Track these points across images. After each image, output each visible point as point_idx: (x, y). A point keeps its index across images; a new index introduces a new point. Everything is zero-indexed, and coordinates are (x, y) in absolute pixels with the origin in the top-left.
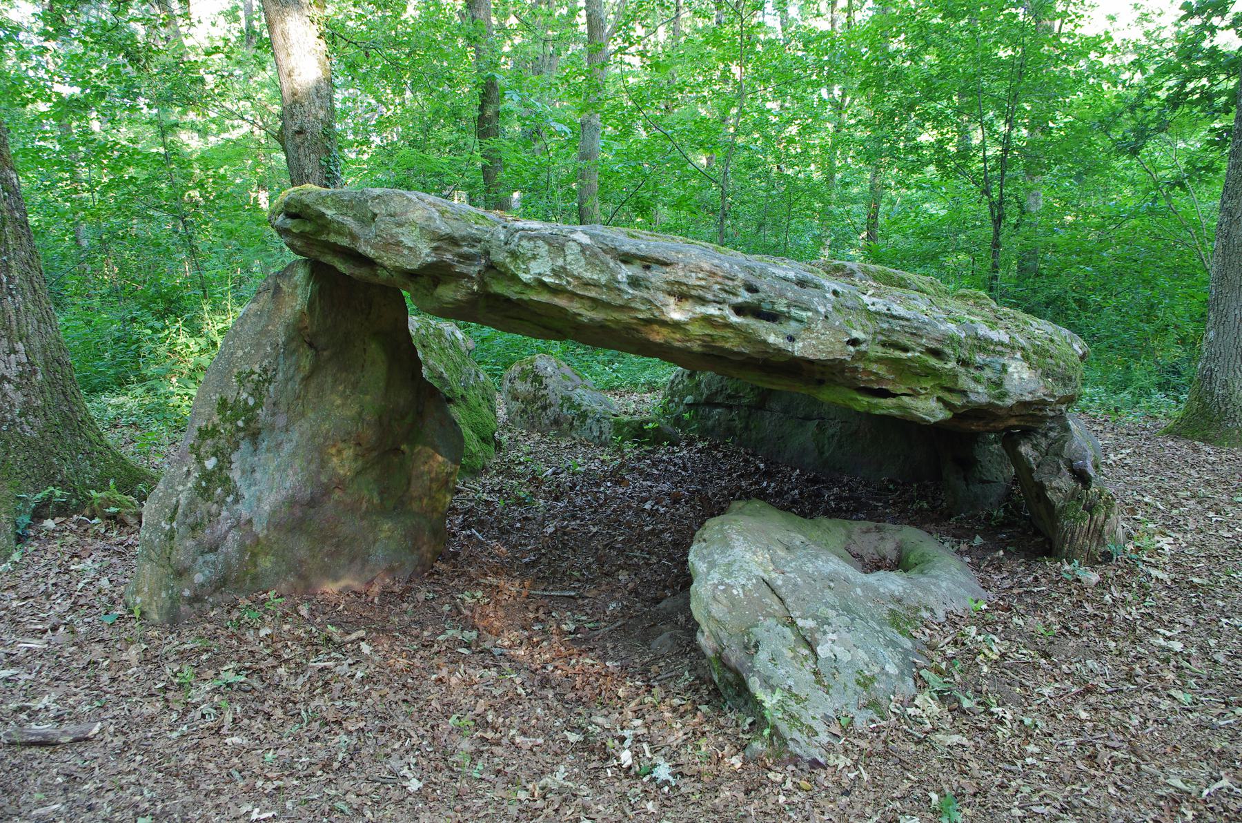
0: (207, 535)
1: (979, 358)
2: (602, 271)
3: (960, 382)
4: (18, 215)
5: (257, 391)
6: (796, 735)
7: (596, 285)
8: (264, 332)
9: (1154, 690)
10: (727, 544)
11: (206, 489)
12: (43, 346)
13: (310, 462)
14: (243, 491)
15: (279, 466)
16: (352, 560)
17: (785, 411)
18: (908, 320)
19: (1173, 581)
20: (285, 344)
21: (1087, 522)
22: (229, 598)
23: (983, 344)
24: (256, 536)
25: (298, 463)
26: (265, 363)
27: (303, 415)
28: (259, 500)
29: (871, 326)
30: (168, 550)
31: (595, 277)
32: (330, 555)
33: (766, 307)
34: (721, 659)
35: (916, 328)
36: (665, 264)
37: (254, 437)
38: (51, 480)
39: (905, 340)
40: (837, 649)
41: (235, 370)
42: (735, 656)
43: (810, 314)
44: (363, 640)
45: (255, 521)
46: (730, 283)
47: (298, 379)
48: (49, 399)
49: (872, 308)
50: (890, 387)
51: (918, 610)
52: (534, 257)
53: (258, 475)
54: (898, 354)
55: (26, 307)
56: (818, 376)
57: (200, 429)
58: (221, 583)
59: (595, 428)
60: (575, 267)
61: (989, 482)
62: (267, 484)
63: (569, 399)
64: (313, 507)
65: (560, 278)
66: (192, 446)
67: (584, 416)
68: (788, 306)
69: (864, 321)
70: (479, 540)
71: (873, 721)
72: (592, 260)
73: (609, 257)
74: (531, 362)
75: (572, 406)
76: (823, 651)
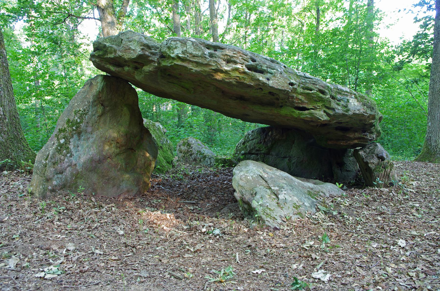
0: (59, 167)
1: (339, 96)
2: (199, 51)
3: (332, 105)
4: (5, 65)
5: (81, 117)
6: (269, 219)
7: (197, 56)
8: (85, 98)
9: (407, 214)
10: (247, 165)
11: (60, 150)
12: (9, 110)
13: (99, 146)
14: (74, 153)
15: (88, 146)
16: (114, 186)
17: (277, 155)
18: (312, 79)
19: (416, 192)
20: (93, 102)
21: (384, 172)
22: (66, 193)
23: (340, 92)
24: (78, 170)
25: (95, 146)
26: (85, 107)
27: (98, 129)
28: (79, 157)
29: (298, 80)
30: (44, 171)
31: (197, 53)
32: (106, 183)
33: (259, 67)
34: (242, 199)
35: (315, 82)
36: (222, 49)
37: (79, 134)
38: (8, 157)
39: (311, 86)
40: (286, 196)
41: (74, 110)
42: (247, 197)
43: (275, 71)
44: (113, 207)
45: (77, 165)
46: (245, 57)
47: (97, 115)
48: (10, 129)
49: (299, 74)
50: (306, 106)
51: (319, 192)
52: (176, 48)
53: (80, 148)
54: (308, 91)
55: (5, 96)
56: (281, 105)
57: (59, 129)
58: (63, 186)
59: (209, 161)
60: (190, 50)
61: (349, 171)
62: (83, 152)
63: (200, 151)
64: (100, 163)
65: (185, 54)
66: (56, 135)
67: (205, 157)
68: (267, 67)
69: (295, 78)
70: (162, 189)
71: (299, 218)
72: (196, 47)
73: (202, 46)
74: (187, 139)
75: (201, 154)
76: (281, 197)
